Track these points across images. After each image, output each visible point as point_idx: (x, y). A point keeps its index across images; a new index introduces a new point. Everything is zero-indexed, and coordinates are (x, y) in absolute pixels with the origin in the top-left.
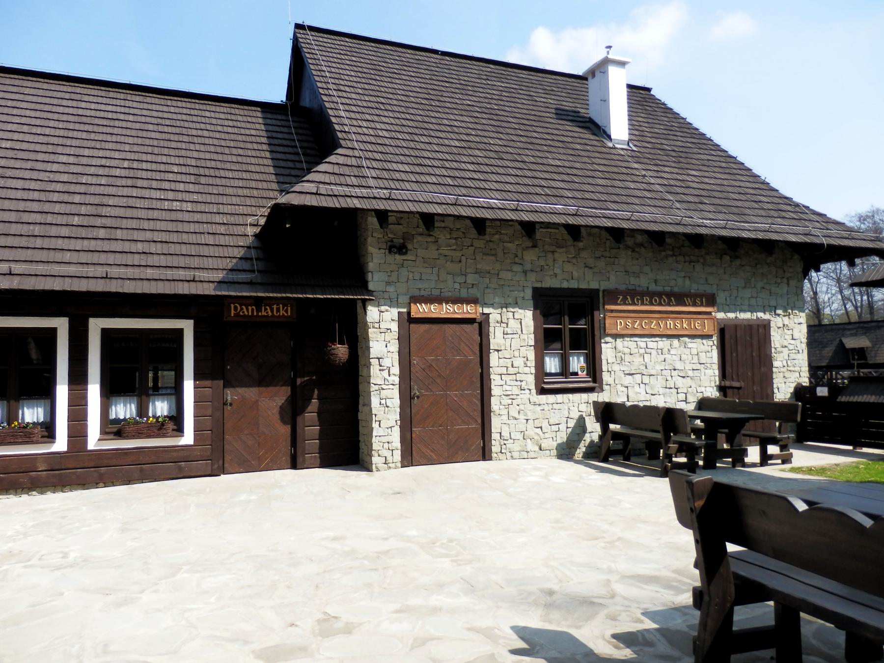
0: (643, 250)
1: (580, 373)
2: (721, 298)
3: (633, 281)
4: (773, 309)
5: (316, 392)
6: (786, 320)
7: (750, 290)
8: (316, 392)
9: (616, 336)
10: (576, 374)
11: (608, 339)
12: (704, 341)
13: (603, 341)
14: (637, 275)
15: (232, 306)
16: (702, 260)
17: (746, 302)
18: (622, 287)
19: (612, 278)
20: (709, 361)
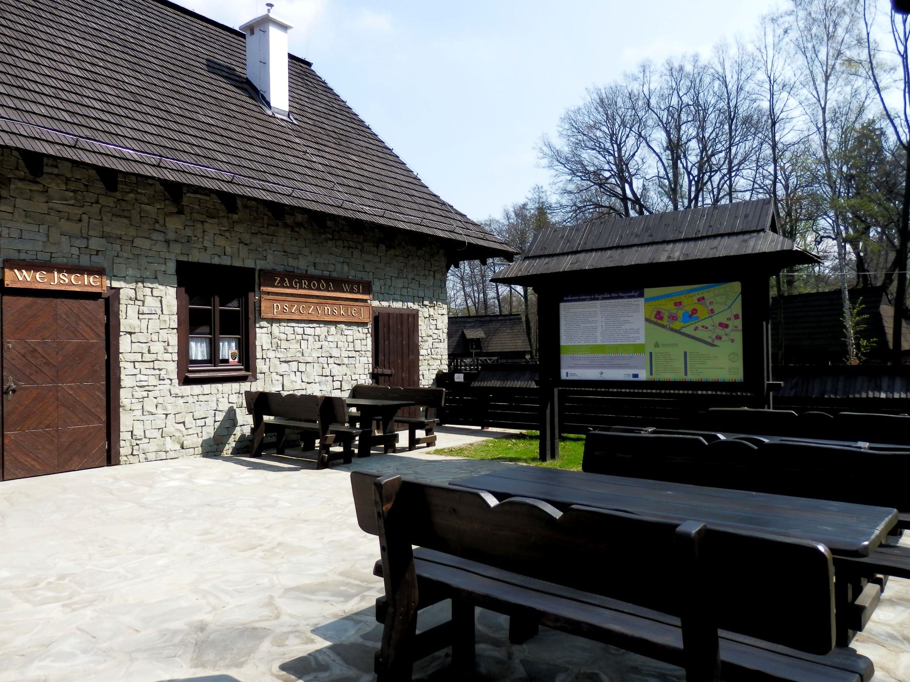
0: (302, 231)
1: (231, 360)
3: (292, 262)
4: (420, 300)
9: (272, 321)
10: (226, 361)
13: (257, 325)
16: (360, 247)
18: (280, 268)
19: (270, 257)
20: (364, 348)
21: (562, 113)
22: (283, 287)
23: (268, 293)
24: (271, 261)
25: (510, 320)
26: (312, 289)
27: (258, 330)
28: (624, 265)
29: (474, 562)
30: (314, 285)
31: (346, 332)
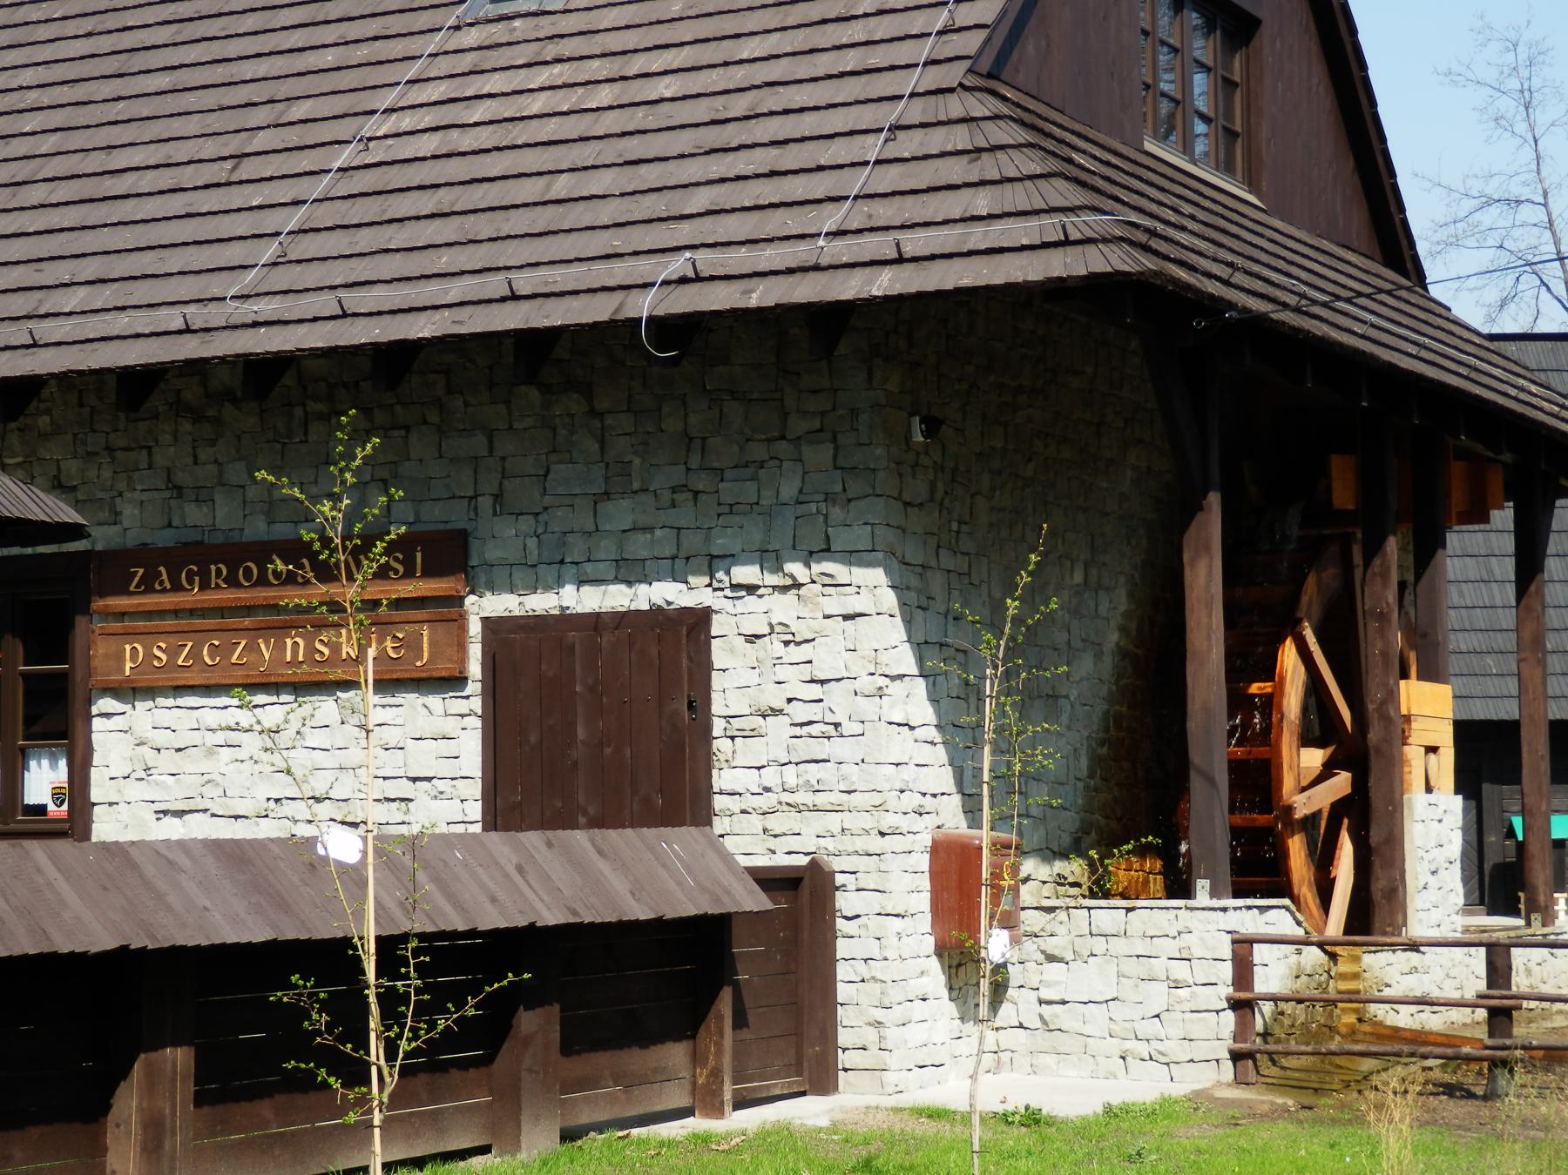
0: (229, 410)
1: (51, 807)
2: (485, 551)
3: (195, 515)
4: (712, 563)
5: (1346, 821)
6: (783, 608)
7: (625, 503)
8: (1346, 821)
9: (131, 691)
10: (41, 809)
11: (105, 704)
12: (434, 701)
13: (94, 710)
14: (203, 496)
15: (213, 567)
16: (434, 418)
17: (607, 549)
18: (165, 539)
19: (129, 512)
20: (447, 769)
21: (1034, 1105)
22: (149, 590)
23: (122, 615)
24: (132, 521)
25: (1527, 368)
26: (238, 585)
27: (97, 723)
28: (1476, 718)
29: (1188, 646)
30: (248, 571)
31: (377, 716)
